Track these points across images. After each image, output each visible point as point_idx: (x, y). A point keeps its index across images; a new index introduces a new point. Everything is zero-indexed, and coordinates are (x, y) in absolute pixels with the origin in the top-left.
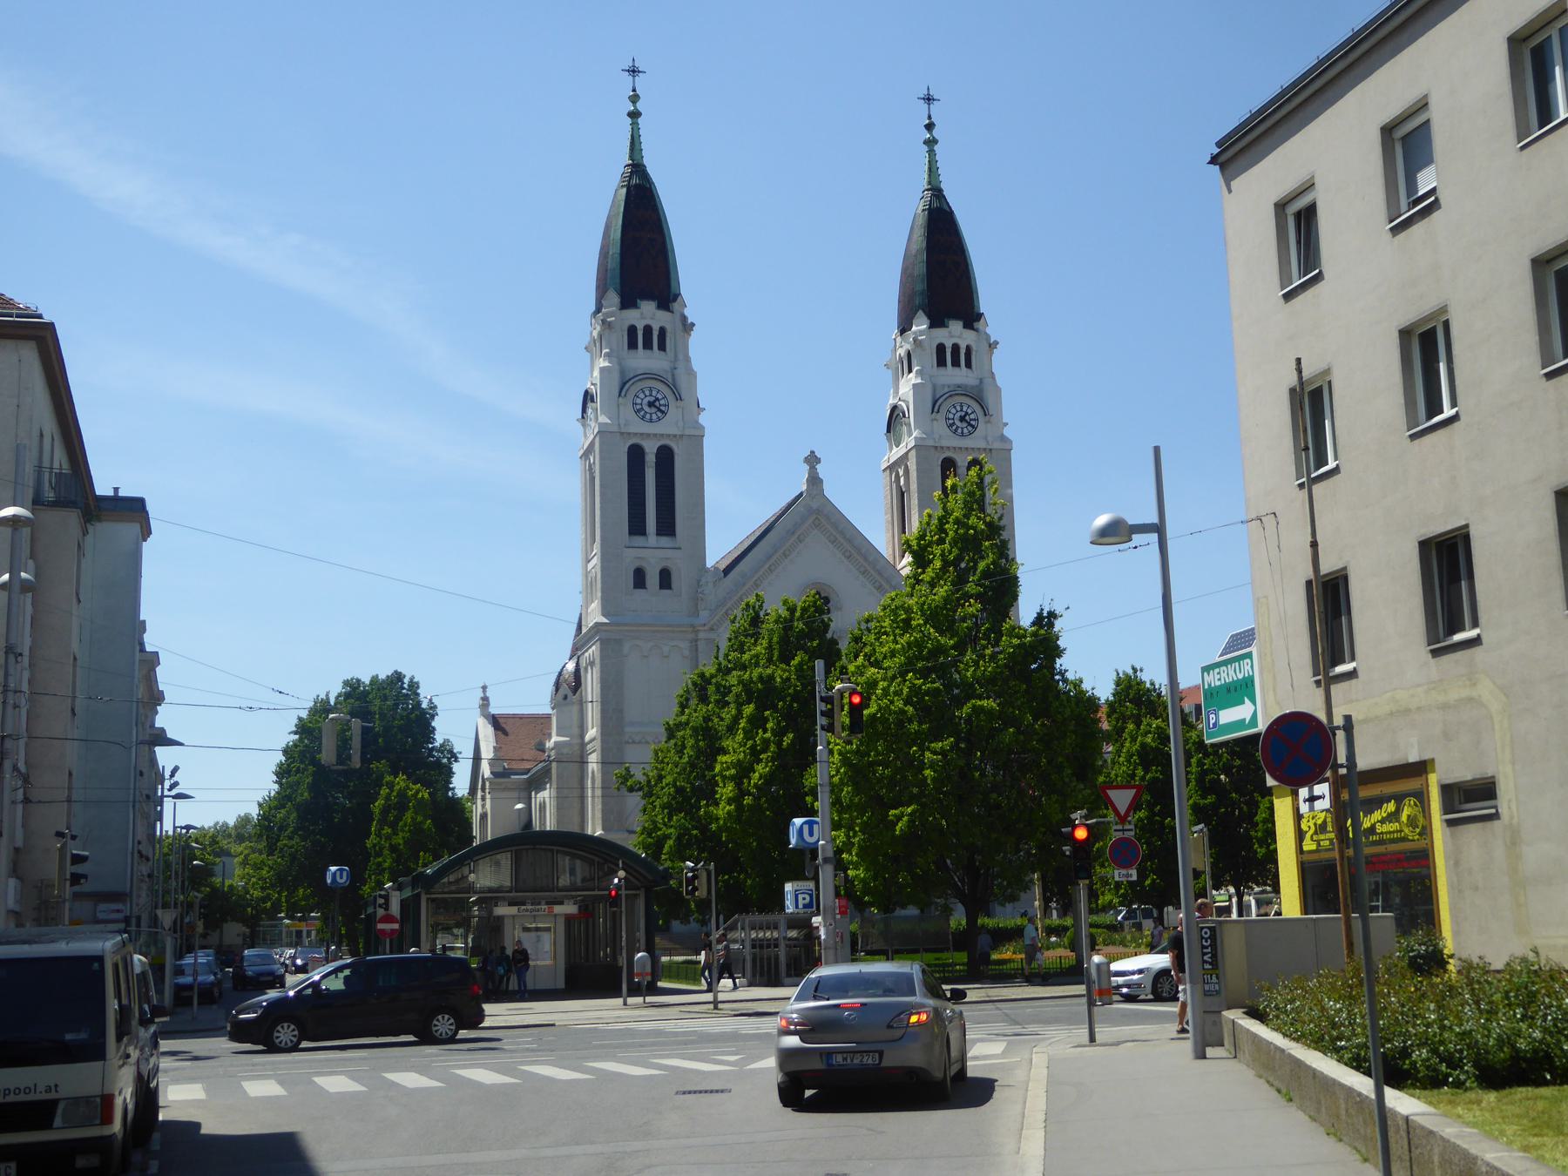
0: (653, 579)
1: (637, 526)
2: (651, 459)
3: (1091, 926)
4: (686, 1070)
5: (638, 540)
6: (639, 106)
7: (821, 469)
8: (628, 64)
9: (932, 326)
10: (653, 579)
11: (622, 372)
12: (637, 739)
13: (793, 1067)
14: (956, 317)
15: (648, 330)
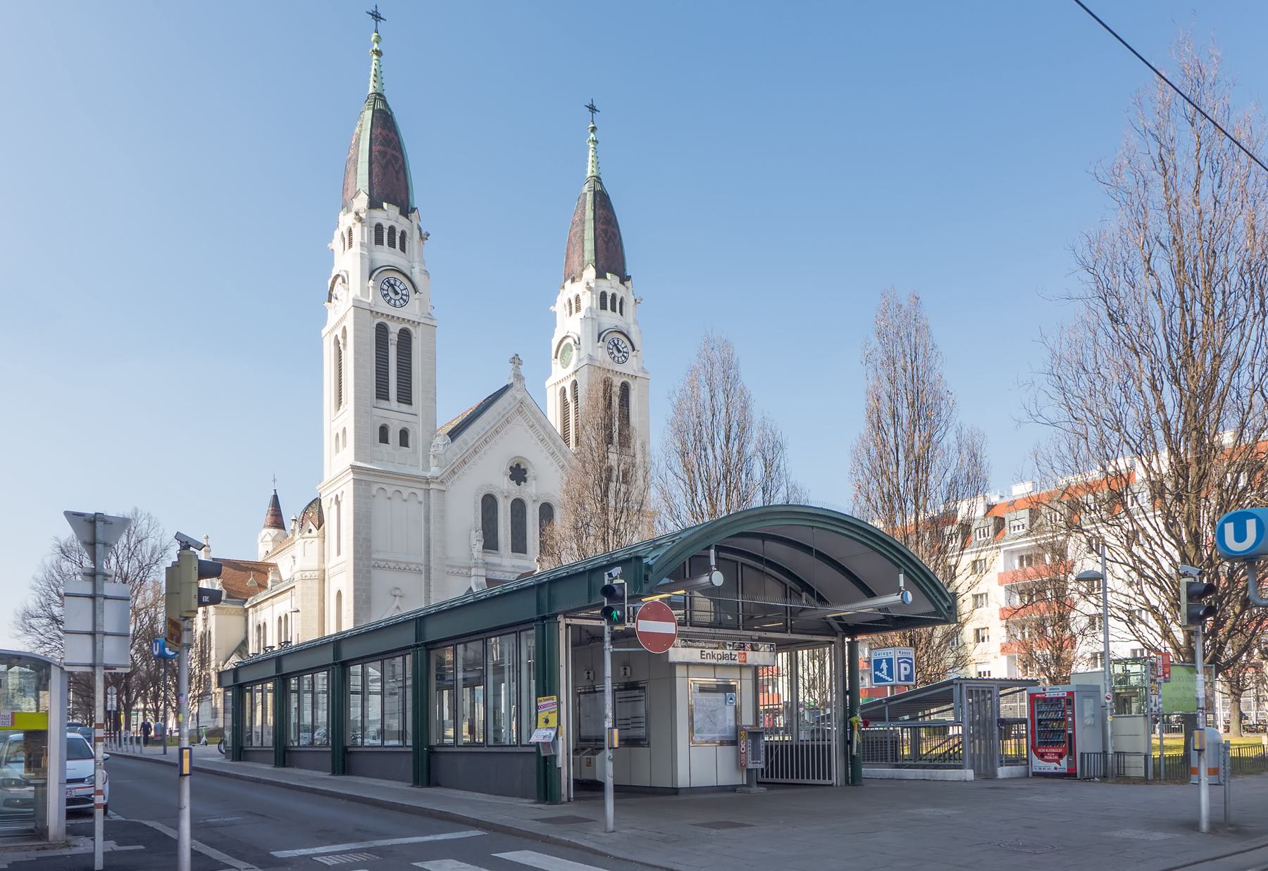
0: (394, 436)
1: (382, 394)
2: (393, 337)
3: (889, 661)
4: (428, 835)
5: (383, 403)
7: (523, 370)
8: (589, 103)
9: (597, 277)
10: (394, 436)
11: (372, 261)
12: (392, 565)
13: (599, 794)
14: (614, 272)
15: (392, 230)
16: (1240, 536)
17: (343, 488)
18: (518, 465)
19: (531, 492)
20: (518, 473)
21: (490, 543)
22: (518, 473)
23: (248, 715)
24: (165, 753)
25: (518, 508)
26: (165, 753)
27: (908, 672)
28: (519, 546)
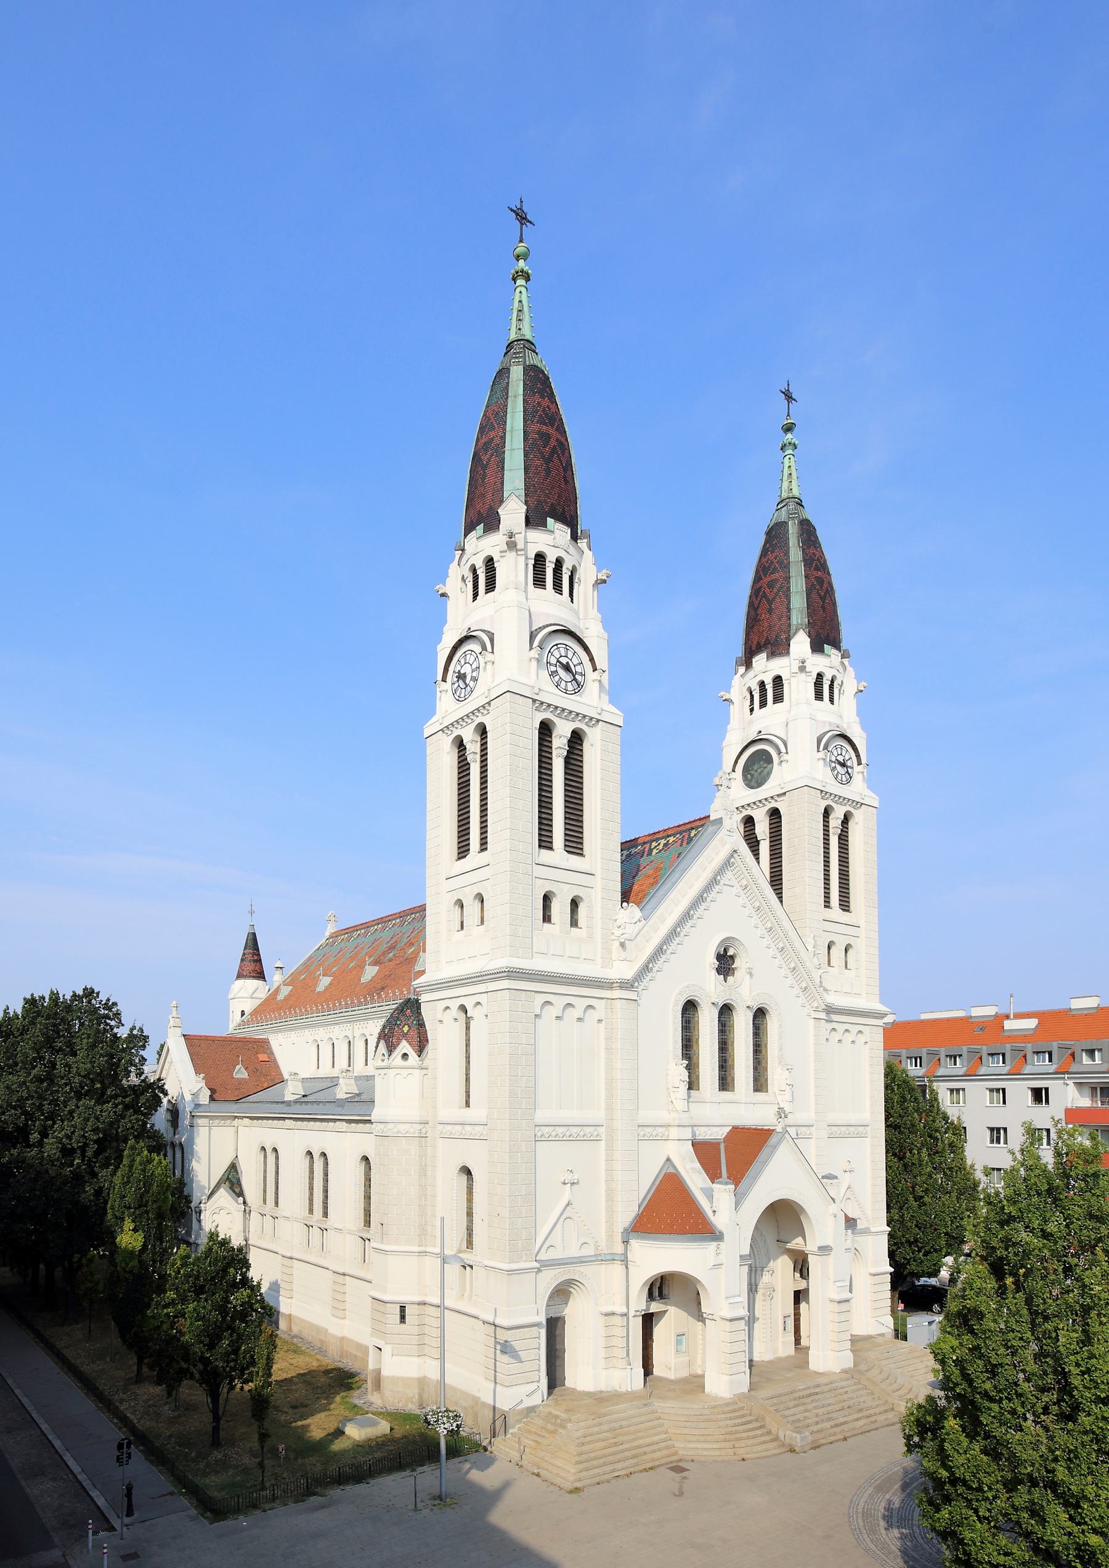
20: (725, 963)
22: (725, 963)
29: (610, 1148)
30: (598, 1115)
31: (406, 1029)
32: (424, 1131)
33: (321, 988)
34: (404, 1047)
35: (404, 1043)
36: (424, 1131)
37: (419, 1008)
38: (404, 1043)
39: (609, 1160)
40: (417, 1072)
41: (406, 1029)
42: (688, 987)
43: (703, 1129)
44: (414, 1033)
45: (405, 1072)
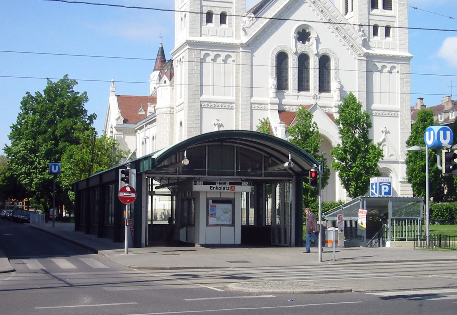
6: (217, 11)
16: (55, 169)
17: (183, 54)
18: (304, 31)
19: (311, 49)
20: (303, 35)
21: (281, 85)
22: (303, 35)
23: (174, 202)
24: (53, 226)
25: (303, 59)
26: (53, 226)
27: (387, 190)
28: (303, 85)
29: (237, 112)
30: (232, 98)
31: (166, 71)
32: (172, 111)
33: (445, 193)
34: (165, 78)
35: (165, 76)
36: (172, 111)
37: (172, 62)
38: (165, 76)
39: (237, 117)
40: (169, 87)
41: (166, 71)
42: (280, 46)
43: (287, 107)
44: (169, 72)
45: (165, 88)
